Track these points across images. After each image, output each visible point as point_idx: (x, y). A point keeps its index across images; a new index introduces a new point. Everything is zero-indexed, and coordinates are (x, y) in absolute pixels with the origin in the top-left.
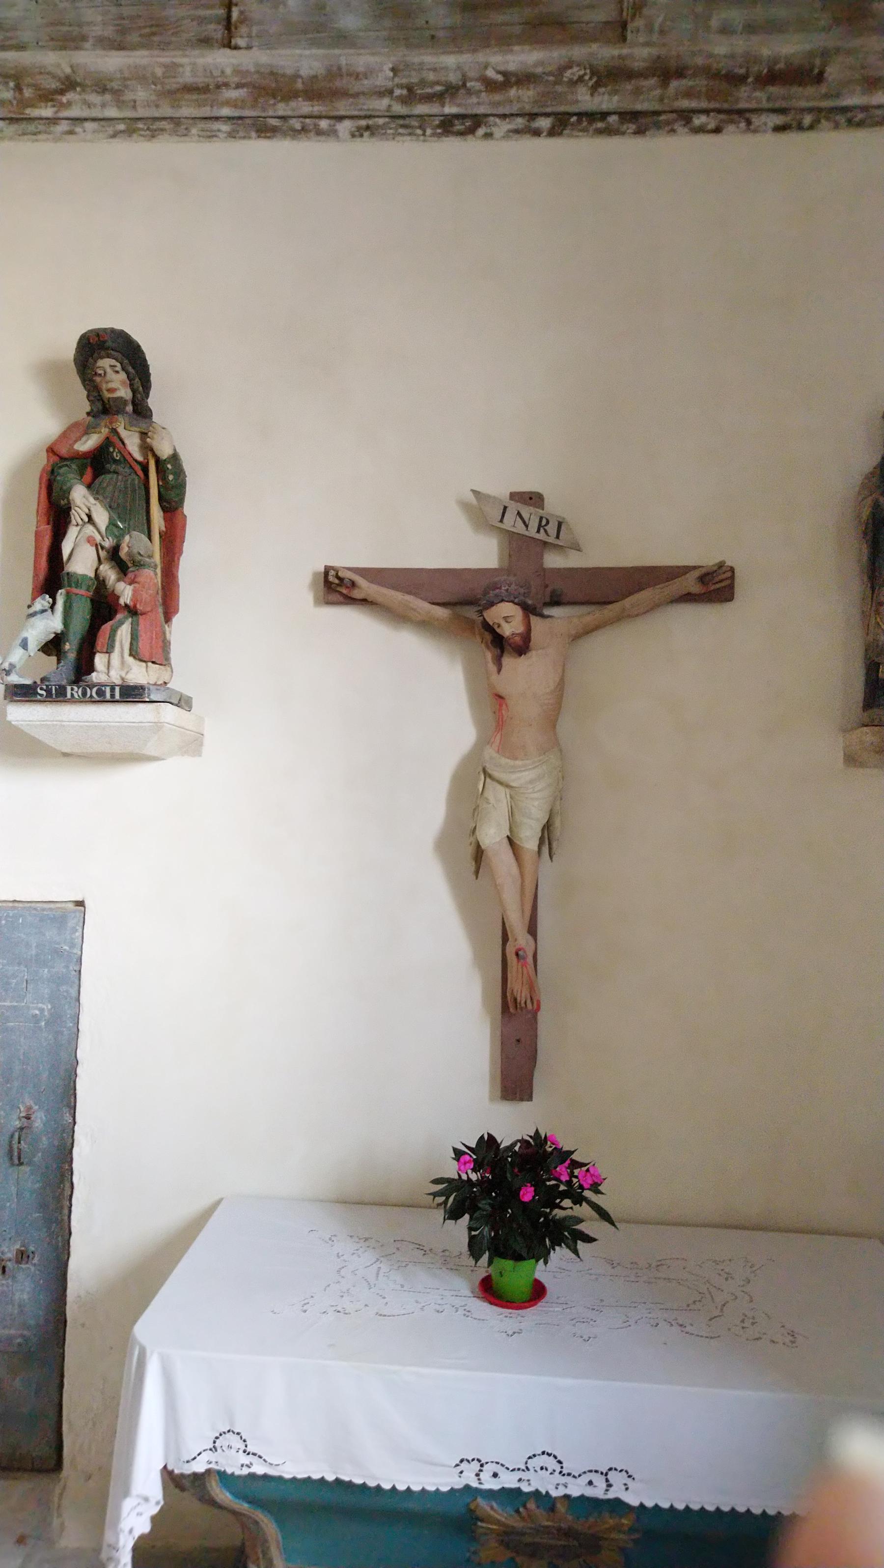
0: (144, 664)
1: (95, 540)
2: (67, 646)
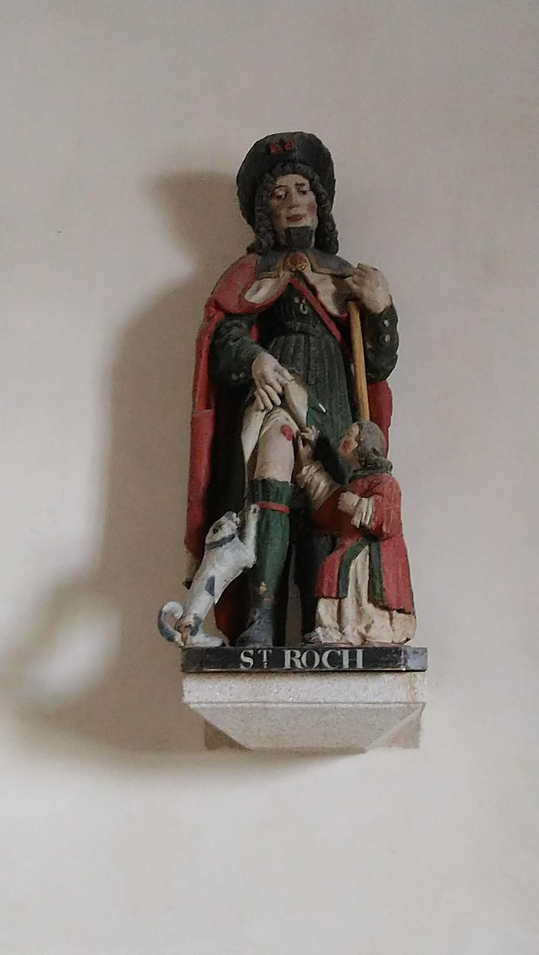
0: (387, 614)
1: (291, 430)
2: (263, 588)
